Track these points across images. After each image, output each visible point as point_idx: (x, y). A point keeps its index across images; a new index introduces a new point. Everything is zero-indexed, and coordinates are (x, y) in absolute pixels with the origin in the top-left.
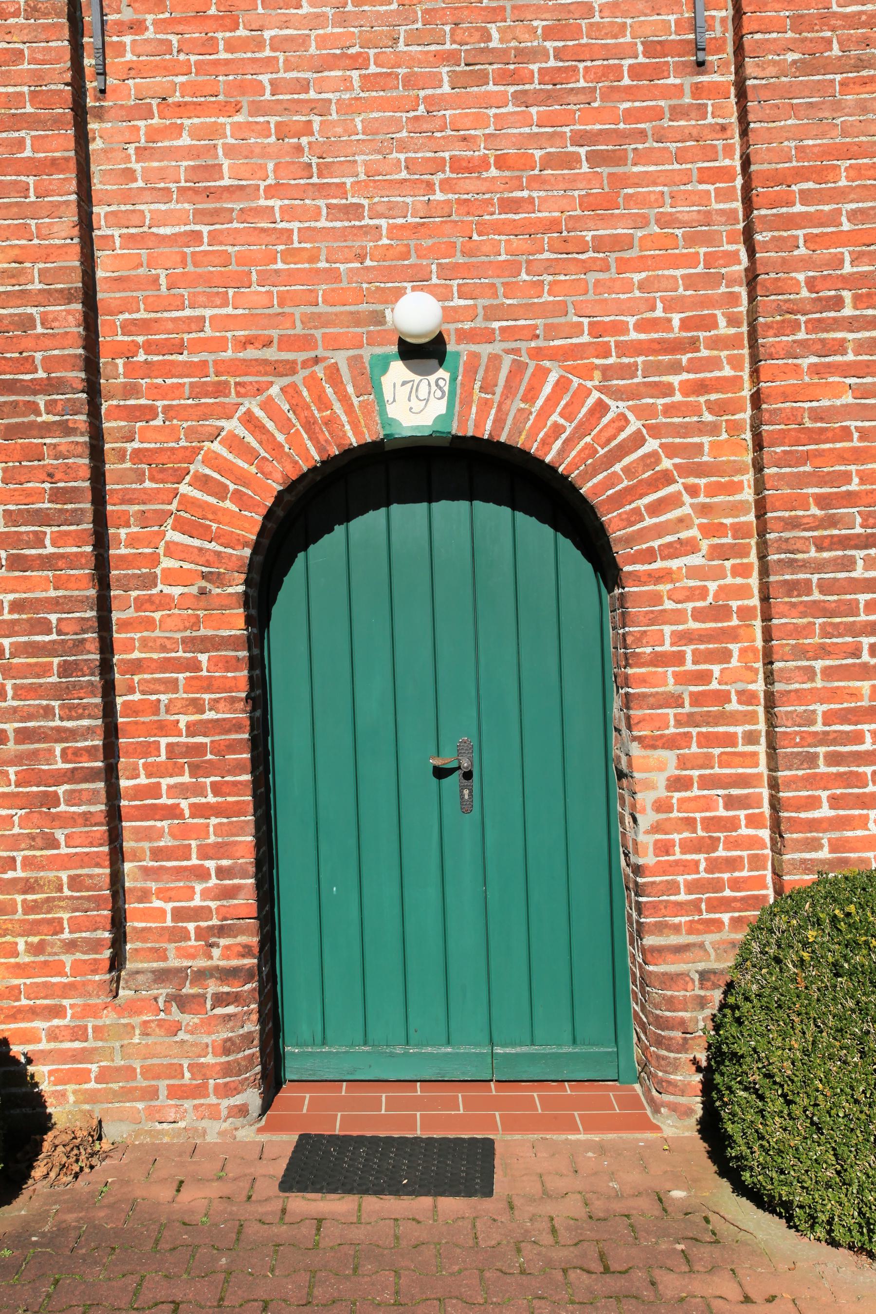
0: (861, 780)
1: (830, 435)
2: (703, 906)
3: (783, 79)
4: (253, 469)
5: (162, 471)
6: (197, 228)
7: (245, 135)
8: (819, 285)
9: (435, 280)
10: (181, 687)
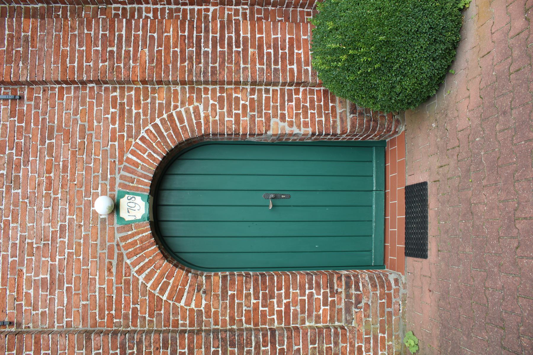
0: (284, 54)
1: (159, 57)
2: (327, 112)
3: (29, 68)
4: (158, 271)
5: (157, 306)
6: (65, 288)
7: (31, 269)
8: (104, 58)
9: (91, 199)
10: (241, 302)
